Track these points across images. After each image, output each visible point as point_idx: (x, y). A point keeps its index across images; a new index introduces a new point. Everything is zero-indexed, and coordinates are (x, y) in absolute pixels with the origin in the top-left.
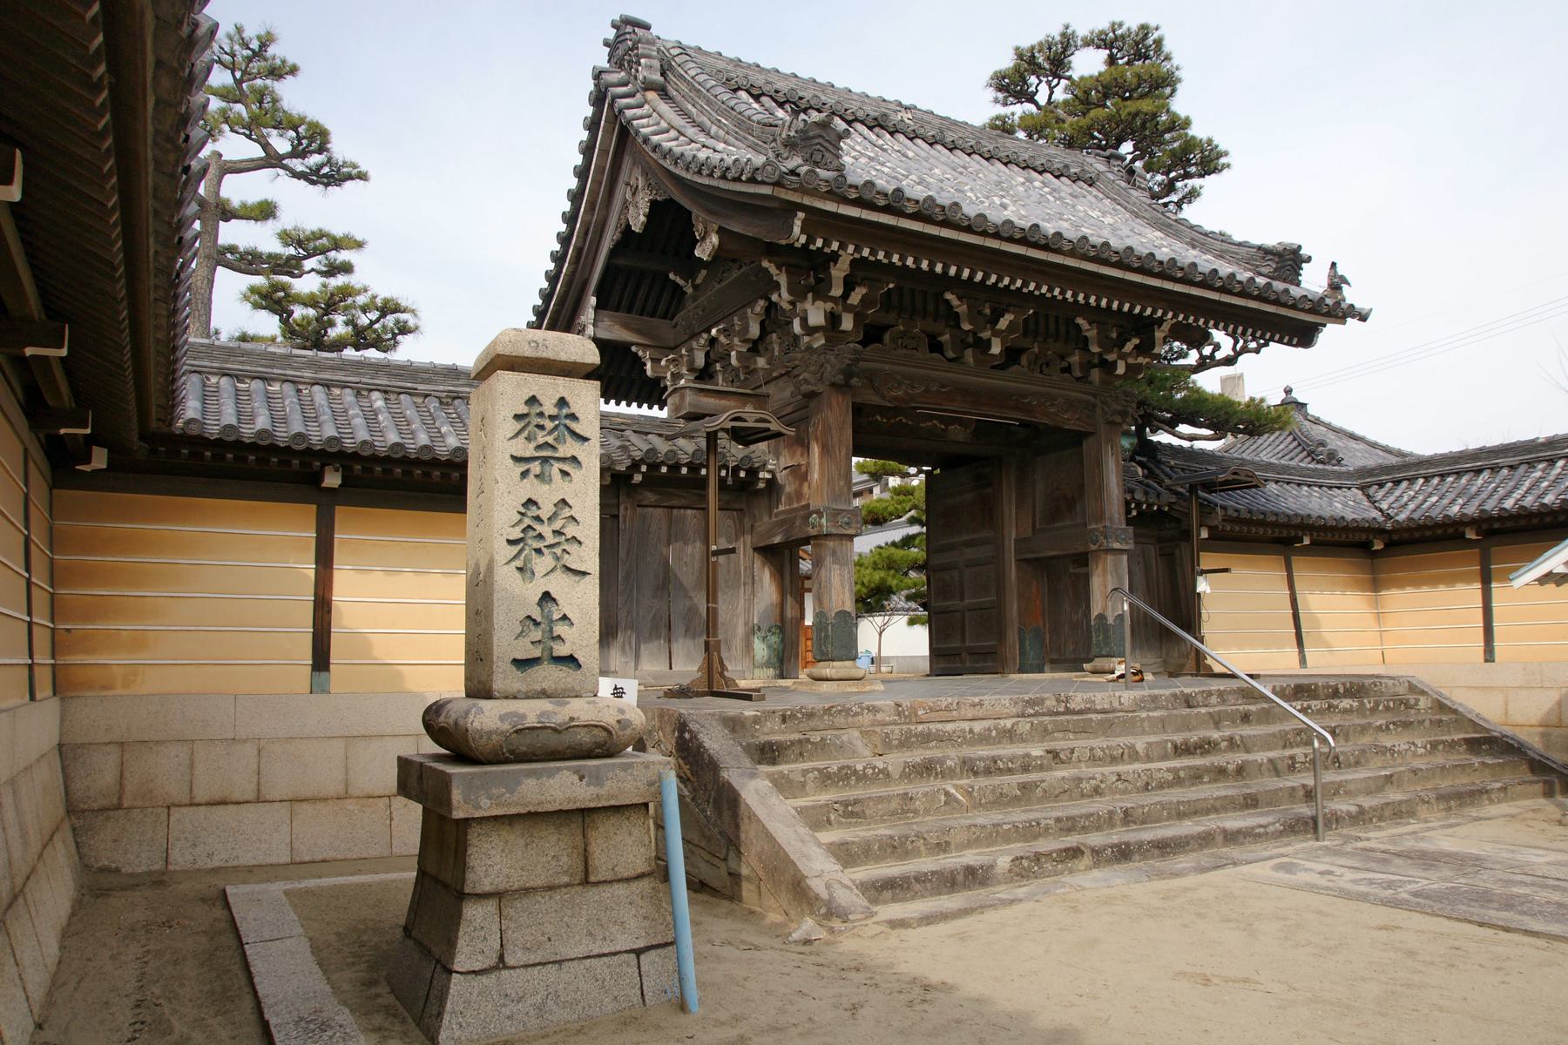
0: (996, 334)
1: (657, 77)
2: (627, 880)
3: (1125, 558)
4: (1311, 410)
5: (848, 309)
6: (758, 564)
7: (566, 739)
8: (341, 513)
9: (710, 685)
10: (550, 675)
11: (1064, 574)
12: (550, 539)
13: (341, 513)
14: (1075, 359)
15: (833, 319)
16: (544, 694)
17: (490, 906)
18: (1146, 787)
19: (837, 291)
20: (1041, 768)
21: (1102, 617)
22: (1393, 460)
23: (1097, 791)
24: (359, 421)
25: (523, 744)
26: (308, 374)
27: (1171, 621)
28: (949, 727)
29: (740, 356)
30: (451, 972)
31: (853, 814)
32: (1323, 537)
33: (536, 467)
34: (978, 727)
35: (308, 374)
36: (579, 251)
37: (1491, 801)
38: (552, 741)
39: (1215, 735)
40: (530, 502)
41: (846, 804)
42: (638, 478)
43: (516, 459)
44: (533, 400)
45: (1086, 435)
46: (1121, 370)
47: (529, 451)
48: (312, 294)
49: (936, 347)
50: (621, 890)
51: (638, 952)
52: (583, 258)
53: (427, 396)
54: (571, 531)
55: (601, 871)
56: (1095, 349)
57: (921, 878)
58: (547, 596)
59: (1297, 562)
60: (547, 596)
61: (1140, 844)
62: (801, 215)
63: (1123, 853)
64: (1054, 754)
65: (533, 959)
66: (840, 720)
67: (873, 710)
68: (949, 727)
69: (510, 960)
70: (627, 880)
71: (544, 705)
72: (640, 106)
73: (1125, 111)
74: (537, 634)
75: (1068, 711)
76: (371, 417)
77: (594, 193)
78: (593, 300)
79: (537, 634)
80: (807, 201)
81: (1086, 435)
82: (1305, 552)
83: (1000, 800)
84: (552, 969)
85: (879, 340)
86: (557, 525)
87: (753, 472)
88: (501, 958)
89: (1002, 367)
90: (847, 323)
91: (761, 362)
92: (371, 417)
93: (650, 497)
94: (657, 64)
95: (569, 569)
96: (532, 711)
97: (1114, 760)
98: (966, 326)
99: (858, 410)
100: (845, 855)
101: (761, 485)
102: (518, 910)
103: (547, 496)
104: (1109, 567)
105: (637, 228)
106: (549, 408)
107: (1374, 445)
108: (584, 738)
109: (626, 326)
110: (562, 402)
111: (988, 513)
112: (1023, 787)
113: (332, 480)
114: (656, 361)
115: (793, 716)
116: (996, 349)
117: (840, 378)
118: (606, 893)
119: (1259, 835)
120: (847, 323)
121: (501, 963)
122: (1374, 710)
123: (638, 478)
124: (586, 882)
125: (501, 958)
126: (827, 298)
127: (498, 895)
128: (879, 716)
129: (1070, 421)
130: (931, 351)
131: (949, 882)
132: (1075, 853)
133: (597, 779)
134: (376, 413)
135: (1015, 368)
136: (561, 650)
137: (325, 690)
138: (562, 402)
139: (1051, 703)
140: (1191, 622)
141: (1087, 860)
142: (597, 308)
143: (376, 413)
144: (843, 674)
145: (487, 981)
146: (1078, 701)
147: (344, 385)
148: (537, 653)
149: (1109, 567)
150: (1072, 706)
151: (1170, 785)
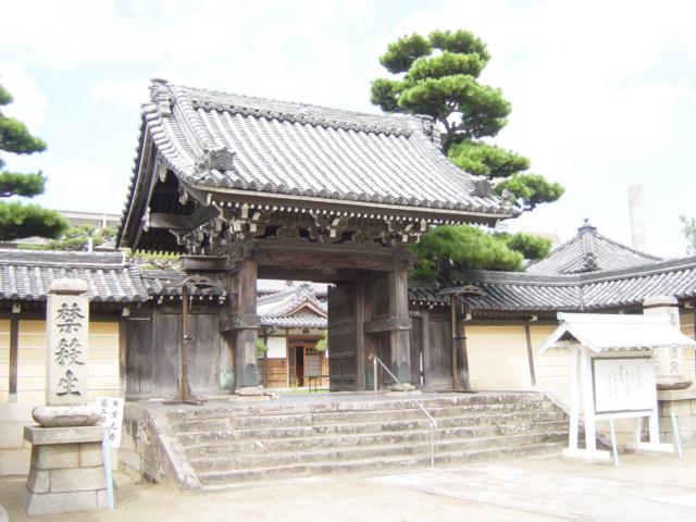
0: (333, 228)
1: (168, 111)
2: (94, 467)
3: (408, 333)
4: (600, 232)
5: (253, 222)
6: (222, 340)
7: (74, 420)
8: (21, 322)
9: (184, 397)
10: (70, 398)
11: (382, 342)
12: (70, 352)
13: (21, 322)
14: (383, 234)
15: (246, 228)
16: (68, 405)
17: (46, 473)
18: (358, 444)
19: (245, 215)
20: (310, 435)
21: (395, 363)
22: (649, 262)
23: (331, 445)
24: (27, 285)
25: (59, 421)
26: (7, 261)
27: (454, 362)
28: (270, 417)
29: (214, 239)
30: (32, 493)
31: (211, 452)
32: (542, 315)
33: (65, 328)
34: (284, 417)
35: (7, 261)
36: (141, 186)
37: (547, 452)
38: (68, 420)
39: (406, 422)
40: (63, 340)
41: (207, 448)
42: (160, 302)
43: (59, 326)
44: (64, 305)
45: (389, 272)
46: (405, 239)
47: (63, 322)
48: (32, 175)
49: (304, 233)
50: (91, 470)
51: (97, 491)
52: (143, 189)
53: (60, 268)
54: (78, 349)
55: (85, 464)
56: (391, 230)
57: (228, 476)
58: (69, 372)
59: (533, 329)
60: (69, 372)
61: (337, 467)
62: (210, 195)
63: (328, 470)
64: (318, 430)
65: (62, 490)
66: (222, 414)
67: (239, 410)
68: (270, 417)
69: (52, 490)
70: (94, 467)
71: (67, 408)
72: (159, 125)
73: (441, 87)
74: (65, 384)
75: (338, 411)
76: (33, 281)
77: (145, 160)
78: (148, 209)
79: (65, 384)
80: (211, 189)
81: (389, 272)
82: (535, 323)
83: (281, 448)
84: (66, 495)
85: (274, 234)
86: (73, 347)
87: (216, 297)
88: (50, 488)
89: (340, 242)
90: (253, 228)
91: (224, 242)
92: (33, 281)
93: (168, 309)
94: (168, 103)
95: (77, 362)
96: (62, 411)
97: (358, 432)
98: (318, 225)
99: (259, 267)
100: (198, 467)
101: (221, 303)
102: (56, 473)
103: (69, 337)
104: (399, 338)
105: (163, 180)
106: (70, 307)
107: (641, 255)
108: (80, 420)
109: (167, 221)
110: (75, 305)
111: (352, 311)
112: (292, 443)
113: (16, 310)
114: (181, 237)
115: (200, 413)
116: (333, 234)
117: (249, 255)
118: (86, 471)
119: (403, 465)
120: (253, 228)
121: (49, 492)
122: (512, 410)
123: (160, 302)
124: (79, 467)
125: (50, 488)
126: (241, 219)
127: (49, 470)
128: (241, 413)
129: (376, 266)
130: (302, 236)
131: (242, 477)
132: (303, 469)
133: (83, 433)
134: (36, 278)
135: (348, 242)
136: (74, 390)
137: (15, 401)
138: (75, 305)
139: (329, 407)
140: (462, 363)
141: (307, 472)
142: (150, 213)
143: (36, 278)
144: (250, 393)
145: (46, 496)
146: (343, 406)
147: (22, 265)
148: (65, 391)
149: (399, 338)
150: (340, 408)
151: (371, 443)
